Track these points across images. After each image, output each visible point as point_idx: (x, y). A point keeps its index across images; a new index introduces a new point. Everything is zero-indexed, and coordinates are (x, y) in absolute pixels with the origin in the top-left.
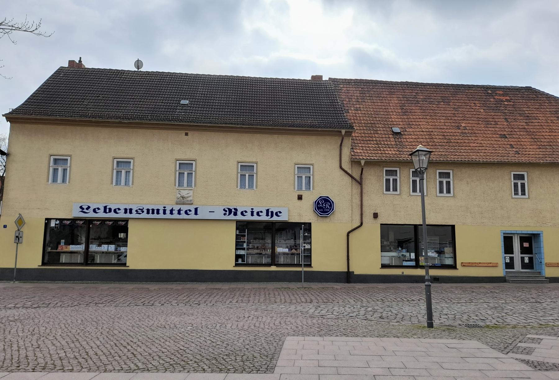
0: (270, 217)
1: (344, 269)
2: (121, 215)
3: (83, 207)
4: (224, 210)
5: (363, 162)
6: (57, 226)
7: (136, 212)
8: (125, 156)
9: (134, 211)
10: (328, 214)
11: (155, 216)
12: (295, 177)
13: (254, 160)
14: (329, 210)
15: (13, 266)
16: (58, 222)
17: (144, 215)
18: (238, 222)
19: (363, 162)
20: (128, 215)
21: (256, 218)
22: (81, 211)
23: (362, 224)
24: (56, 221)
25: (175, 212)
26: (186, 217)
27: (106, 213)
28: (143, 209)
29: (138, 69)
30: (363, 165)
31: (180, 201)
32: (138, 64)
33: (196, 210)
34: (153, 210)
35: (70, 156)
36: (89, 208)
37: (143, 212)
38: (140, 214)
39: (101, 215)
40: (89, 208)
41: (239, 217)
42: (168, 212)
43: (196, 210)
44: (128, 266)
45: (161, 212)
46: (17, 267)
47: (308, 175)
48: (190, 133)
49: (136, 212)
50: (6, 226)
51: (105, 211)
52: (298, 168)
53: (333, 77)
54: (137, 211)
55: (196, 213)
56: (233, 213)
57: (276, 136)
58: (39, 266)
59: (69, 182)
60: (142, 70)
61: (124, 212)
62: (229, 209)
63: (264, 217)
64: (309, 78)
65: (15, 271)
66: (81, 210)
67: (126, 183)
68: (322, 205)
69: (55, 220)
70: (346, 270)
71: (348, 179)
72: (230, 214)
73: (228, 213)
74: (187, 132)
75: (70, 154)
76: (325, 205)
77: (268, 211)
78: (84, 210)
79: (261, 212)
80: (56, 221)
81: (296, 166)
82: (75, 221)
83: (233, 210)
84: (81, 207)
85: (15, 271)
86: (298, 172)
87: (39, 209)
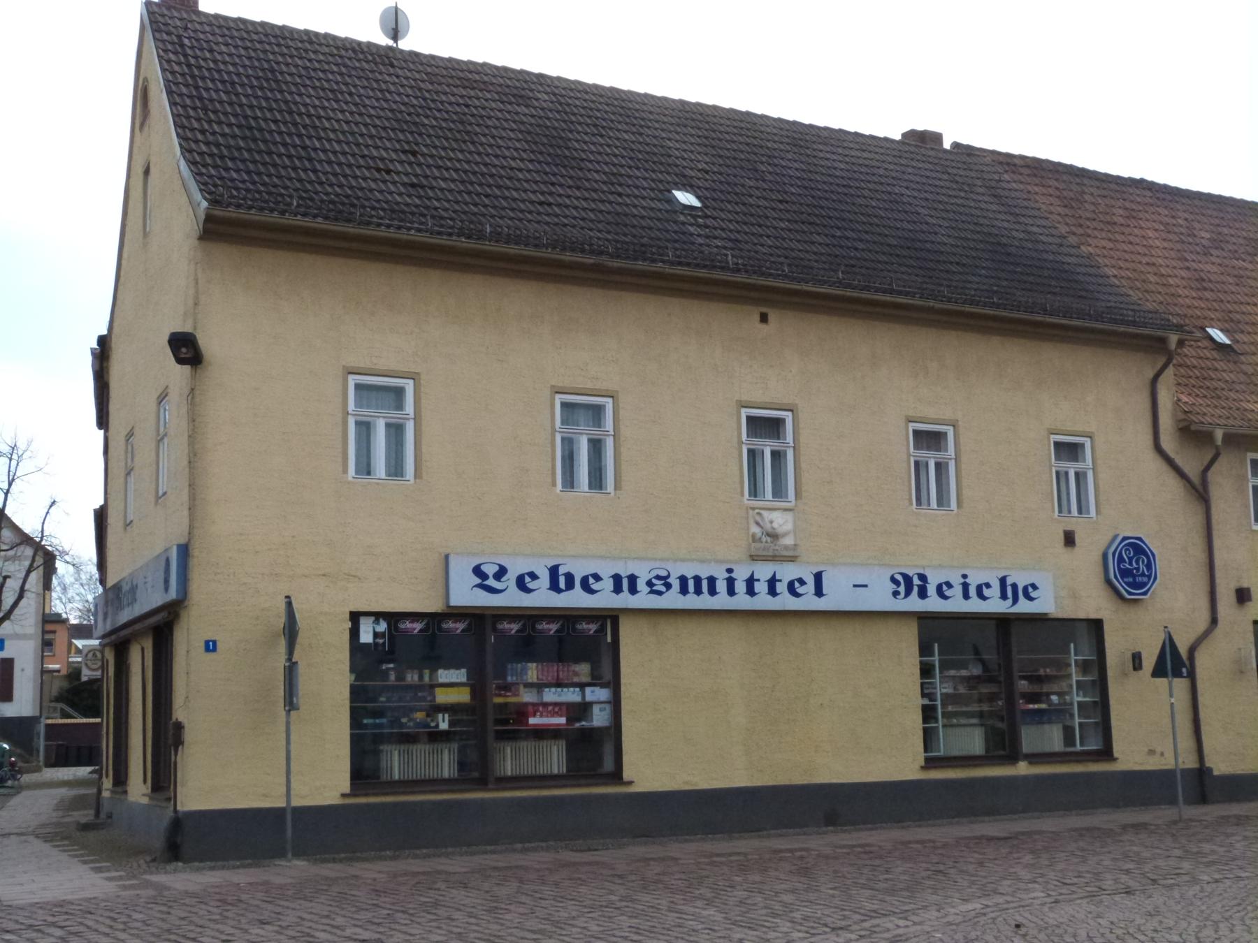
0: (1010, 601)
1: (1188, 761)
2: (604, 598)
3: (484, 568)
4: (893, 580)
5: (1219, 434)
6: (381, 641)
7: (649, 589)
8: (590, 385)
9: (641, 585)
10: (1130, 593)
11: (705, 601)
12: (345, 423)
13: (948, 414)
14: (1145, 579)
15: (281, 803)
16: (382, 627)
17: (672, 600)
18: (924, 618)
19: (1219, 434)
20: (625, 600)
21: (975, 605)
22: (479, 586)
23: (1214, 621)
24: (377, 622)
25: (762, 587)
26: (791, 603)
27: (559, 591)
28: (669, 576)
29: (395, 36)
30: (1219, 442)
31: (764, 549)
32: (395, 24)
33: (818, 577)
34: (683, 580)
35: (414, 377)
36: (501, 573)
37: (668, 586)
38: (660, 593)
39: (542, 597)
40: (501, 573)
41: (933, 604)
42: (740, 587)
43: (818, 577)
44: (630, 783)
45: (721, 586)
46: (296, 802)
47: (394, 416)
48: (773, 316)
49: (649, 589)
50: (214, 642)
51: (554, 587)
52: (358, 387)
53: (964, 141)
54: (650, 584)
55: (819, 592)
56: (916, 589)
57: (996, 341)
58: (344, 795)
59: (417, 475)
60: (405, 44)
61: (548, 586)
62: (905, 576)
63: (995, 605)
64: (898, 137)
65: (289, 817)
66: (478, 581)
67: (942, 500)
68: (1131, 564)
69: (373, 618)
70: (1195, 765)
71: (1172, 483)
72: (908, 592)
73: (902, 589)
74: (764, 310)
75: (413, 368)
76: (1137, 563)
77: (554, 571)
78: (486, 583)
79: (988, 585)
80: (377, 622)
81: (558, 399)
82: (440, 622)
83: (916, 581)
84: (477, 571)
85: (289, 817)
86: (358, 404)
87: (324, 575)
